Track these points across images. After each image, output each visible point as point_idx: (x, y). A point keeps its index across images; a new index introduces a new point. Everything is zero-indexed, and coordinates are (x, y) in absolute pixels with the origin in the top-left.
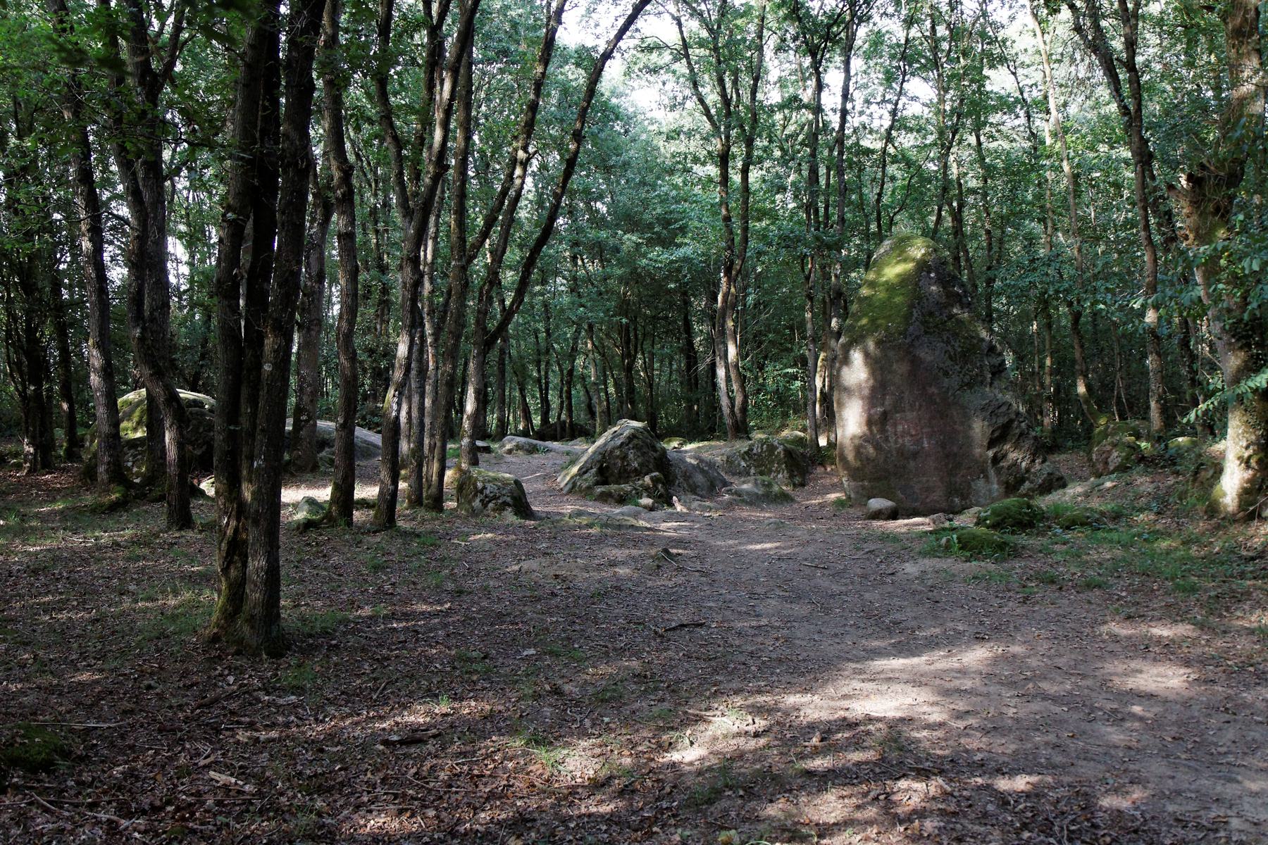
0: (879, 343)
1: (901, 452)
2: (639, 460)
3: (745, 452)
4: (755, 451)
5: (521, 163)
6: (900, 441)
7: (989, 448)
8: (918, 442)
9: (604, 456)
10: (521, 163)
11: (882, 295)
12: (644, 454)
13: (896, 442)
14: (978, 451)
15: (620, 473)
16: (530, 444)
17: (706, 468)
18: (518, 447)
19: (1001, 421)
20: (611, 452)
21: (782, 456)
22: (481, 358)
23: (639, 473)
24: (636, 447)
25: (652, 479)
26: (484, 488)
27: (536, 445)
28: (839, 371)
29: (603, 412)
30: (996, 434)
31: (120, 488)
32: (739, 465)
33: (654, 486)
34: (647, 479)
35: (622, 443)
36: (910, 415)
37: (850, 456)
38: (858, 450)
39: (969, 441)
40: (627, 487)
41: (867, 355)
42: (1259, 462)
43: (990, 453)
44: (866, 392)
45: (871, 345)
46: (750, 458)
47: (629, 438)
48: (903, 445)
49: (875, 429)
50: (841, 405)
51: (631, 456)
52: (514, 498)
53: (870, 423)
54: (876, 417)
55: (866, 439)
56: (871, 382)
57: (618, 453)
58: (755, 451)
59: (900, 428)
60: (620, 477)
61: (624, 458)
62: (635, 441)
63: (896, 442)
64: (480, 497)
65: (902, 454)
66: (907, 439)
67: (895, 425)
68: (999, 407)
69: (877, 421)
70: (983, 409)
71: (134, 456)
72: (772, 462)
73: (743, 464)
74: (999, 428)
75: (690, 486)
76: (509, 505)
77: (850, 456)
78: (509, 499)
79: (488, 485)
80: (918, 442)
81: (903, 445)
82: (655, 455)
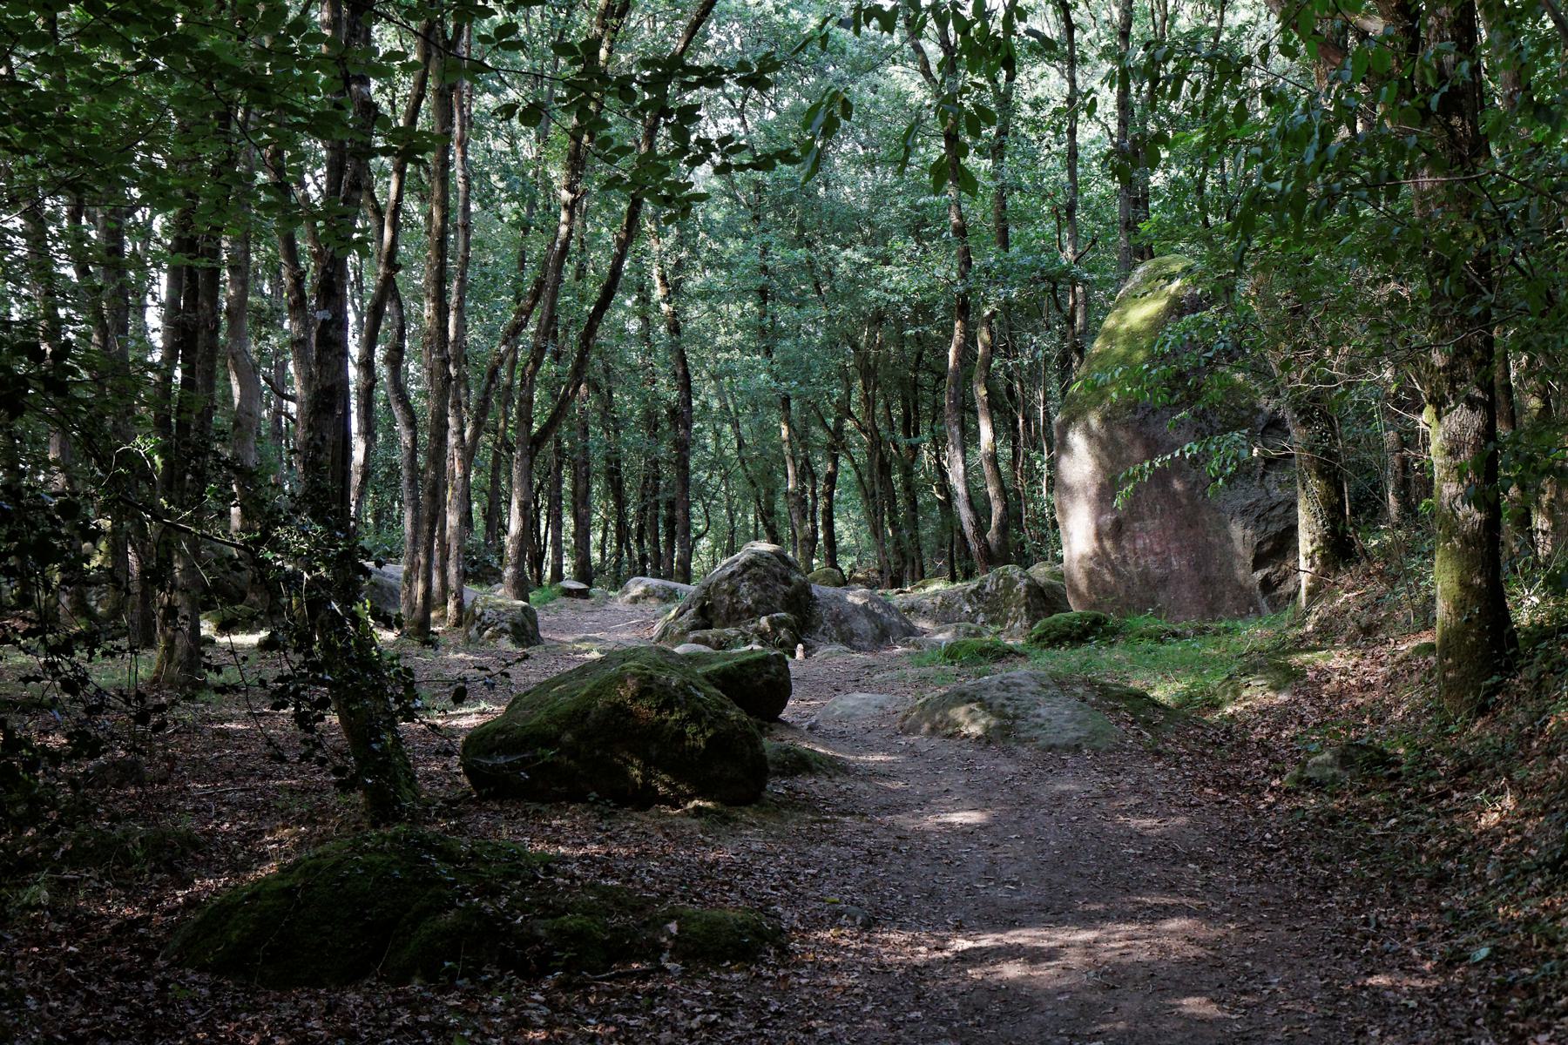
0: (1105, 420)
1: (1145, 575)
2: (756, 595)
3: (972, 591)
4: (987, 589)
5: (566, 206)
6: (1142, 562)
7: (1256, 568)
8: (1165, 562)
9: (707, 593)
10: (566, 206)
11: (1120, 349)
12: (765, 588)
13: (1137, 564)
14: (1240, 573)
15: (728, 613)
16: (665, 589)
17: (879, 611)
18: (647, 594)
19: (1273, 528)
20: (717, 585)
21: (1023, 594)
22: (527, 461)
23: (753, 613)
24: (755, 579)
25: (771, 621)
26: (483, 614)
27: (674, 590)
28: (1058, 458)
29: (805, 539)
30: (1266, 547)
31: (84, 620)
32: (961, 609)
33: (773, 630)
34: (764, 621)
35: (733, 574)
36: (1151, 524)
37: (1083, 585)
38: (1090, 574)
39: (1229, 557)
40: (731, 631)
41: (1089, 434)
42: (1323, 557)
43: (1259, 575)
44: (1093, 491)
45: (1094, 420)
46: (980, 599)
47: (744, 565)
48: (1146, 567)
49: (1108, 544)
50: (1064, 512)
51: (744, 590)
52: (515, 625)
53: (1099, 535)
54: (1107, 528)
55: (1100, 557)
56: (1099, 479)
57: (725, 586)
58: (987, 589)
59: (1140, 544)
60: (729, 620)
61: (734, 592)
62: (753, 570)
63: (1137, 564)
64: (478, 624)
65: (1148, 583)
66: (1151, 558)
67: (1133, 539)
68: (1273, 508)
69: (1113, 531)
70: (1244, 513)
71: (99, 594)
72: (1008, 605)
73: (968, 608)
74: (1269, 539)
75: (841, 633)
76: (506, 632)
77: (1083, 585)
78: (507, 626)
79: (487, 611)
80: (1165, 562)
81: (1146, 567)
82: (786, 588)
